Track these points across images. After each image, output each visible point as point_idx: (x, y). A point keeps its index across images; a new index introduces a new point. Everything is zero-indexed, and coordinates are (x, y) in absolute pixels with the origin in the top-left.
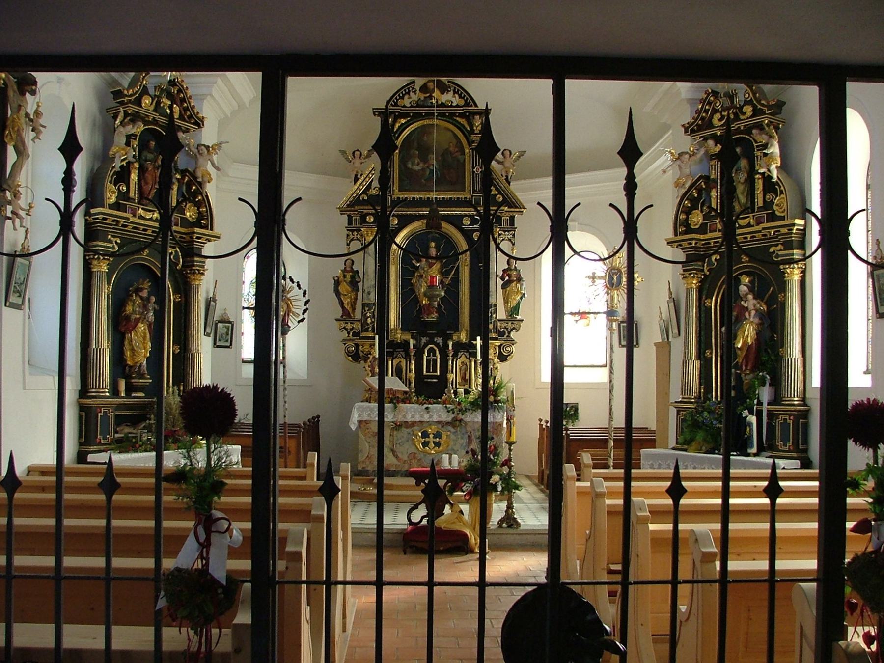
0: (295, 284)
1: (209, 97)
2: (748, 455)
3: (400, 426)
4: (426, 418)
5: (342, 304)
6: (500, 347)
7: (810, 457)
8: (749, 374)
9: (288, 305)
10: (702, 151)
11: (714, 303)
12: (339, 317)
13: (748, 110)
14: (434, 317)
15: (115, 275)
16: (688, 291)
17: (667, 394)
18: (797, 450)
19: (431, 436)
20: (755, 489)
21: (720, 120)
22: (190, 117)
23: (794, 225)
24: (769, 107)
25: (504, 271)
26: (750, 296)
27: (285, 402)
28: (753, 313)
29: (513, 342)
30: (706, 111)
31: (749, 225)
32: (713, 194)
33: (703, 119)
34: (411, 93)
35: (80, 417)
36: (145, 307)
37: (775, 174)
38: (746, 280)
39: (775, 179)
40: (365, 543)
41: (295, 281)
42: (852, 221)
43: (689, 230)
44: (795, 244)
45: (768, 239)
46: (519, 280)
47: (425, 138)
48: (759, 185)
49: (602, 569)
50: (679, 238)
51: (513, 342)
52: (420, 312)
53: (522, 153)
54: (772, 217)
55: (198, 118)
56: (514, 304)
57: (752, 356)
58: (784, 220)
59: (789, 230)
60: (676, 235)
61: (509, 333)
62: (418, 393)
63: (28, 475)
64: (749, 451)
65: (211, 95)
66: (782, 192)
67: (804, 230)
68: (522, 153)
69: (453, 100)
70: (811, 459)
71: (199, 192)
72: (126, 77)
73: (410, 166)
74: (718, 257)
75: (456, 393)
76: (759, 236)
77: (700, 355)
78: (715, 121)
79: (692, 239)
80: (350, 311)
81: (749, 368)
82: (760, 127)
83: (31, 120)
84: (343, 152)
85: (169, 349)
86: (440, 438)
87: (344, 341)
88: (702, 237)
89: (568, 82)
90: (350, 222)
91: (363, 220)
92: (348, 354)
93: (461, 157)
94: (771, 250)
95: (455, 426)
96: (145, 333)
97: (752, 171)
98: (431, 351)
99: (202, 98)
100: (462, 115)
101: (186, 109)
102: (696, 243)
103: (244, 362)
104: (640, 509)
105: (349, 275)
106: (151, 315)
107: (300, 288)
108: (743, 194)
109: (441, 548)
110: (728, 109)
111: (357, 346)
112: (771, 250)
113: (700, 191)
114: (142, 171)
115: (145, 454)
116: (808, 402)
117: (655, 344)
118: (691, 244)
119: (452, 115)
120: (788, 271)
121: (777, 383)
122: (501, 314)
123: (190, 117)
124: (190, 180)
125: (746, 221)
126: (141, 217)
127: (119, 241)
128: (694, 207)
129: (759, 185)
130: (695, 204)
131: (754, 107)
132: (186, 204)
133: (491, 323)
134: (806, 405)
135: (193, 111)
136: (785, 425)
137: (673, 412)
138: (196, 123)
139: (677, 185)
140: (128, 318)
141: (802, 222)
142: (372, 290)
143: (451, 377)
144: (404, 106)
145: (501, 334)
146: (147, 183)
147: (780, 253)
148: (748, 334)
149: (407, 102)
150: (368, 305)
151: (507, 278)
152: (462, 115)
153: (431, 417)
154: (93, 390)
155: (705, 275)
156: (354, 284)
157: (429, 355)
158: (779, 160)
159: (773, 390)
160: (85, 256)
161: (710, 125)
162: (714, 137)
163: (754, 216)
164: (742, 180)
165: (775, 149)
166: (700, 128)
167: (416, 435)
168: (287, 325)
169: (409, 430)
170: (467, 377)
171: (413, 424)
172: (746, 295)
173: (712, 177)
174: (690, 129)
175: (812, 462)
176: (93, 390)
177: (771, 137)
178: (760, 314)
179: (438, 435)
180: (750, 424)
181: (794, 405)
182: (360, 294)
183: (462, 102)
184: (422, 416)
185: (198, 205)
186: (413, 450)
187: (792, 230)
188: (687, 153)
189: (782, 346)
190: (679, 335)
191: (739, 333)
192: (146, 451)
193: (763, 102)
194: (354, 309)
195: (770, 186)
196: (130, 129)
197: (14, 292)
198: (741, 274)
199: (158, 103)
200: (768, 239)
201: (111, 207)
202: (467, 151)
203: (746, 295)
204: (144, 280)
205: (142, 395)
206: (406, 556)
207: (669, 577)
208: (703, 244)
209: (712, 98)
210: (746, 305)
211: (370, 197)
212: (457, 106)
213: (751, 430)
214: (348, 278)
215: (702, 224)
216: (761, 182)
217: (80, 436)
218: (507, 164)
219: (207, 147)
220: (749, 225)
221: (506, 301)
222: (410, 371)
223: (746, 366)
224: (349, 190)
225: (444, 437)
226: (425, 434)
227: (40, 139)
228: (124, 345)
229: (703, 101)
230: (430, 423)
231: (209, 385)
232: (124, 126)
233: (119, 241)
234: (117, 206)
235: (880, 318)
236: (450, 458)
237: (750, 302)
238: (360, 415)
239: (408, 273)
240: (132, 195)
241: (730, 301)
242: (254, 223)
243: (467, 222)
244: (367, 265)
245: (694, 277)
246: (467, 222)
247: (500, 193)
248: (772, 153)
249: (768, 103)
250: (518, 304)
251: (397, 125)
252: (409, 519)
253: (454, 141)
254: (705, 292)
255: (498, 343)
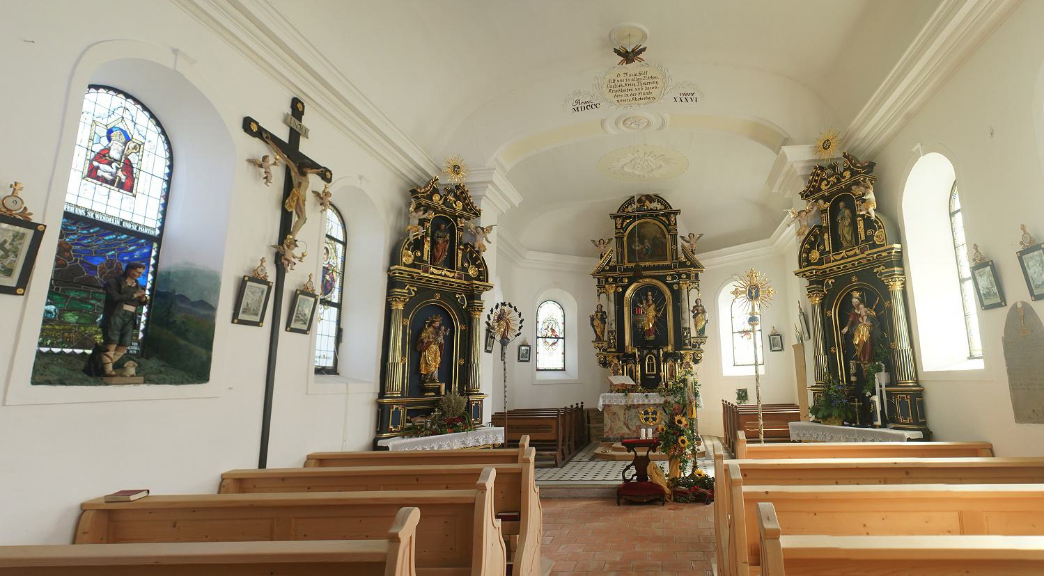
0: (518, 332)
1: (484, 197)
2: (875, 427)
3: (630, 407)
4: (646, 402)
5: (595, 332)
6: (693, 354)
7: (929, 428)
8: (867, 364)
9: (507, 323)
10: (815, 209)
11: (834, 313)
12: (594, 340)
13: (847, 174)
14: (652, 337)
15: (910, 107)
16: (813, 306)
17: (805, 380)
18: (916, 422)
19: (650, 413)
20: (896, 466)
21: (826, 185)
22: (471, 209)
23: (893, 248)
24: (863, 168)
25: (694, 307)
26: (862, 306)
27: (505, 397)
28: (865, 318)
29: (702, 351)
30: (816, 181)
31: (855, 255)
32: (826, 236)
33: (814, 187)
34: (633, 204)
35: (378, 412)
36: (437, 334)
37: (873, 214)
38: (856, 294)
39: (873, 218)
40: (593, 496)
41: (522, 317)
42: (338, 368)
43: (810, 264)
44: (894, 263)
45: (872, 263)
46: (704, 312)
47: (642, 231)
48: (861, 225)
49: (744, 563)
50: (803, 270)
51: (702, 351)
52: (644, 335)
53: (701, 235)
54: (874, 246)
55: (476, 210)
56: (701, 327)
57: (868, 350)
58: (616, 271)
59: (881, 255)
60: (801, 268)
61: (699, 345)
62: (642, 385)
63: (305, 466)
64: (875, 423)
65: (491, 182)
66: (880, 227)
67: (901, 252)
68: (701, 235)
69: (657, 206)
70: (931, 430)
71: (477, 258)
72: (183, 305)
73: (633, 247)
74: (834, 281)
75: (666, 385)
76: (864, 261)
77: (827, 351)
78: (823, 187)
79: (812, 270)
80: (601, 336)
81: (866, 359)
82: (857, 183)
83: (322, 198)
84: (593, 241)
85: (457, 361)
86: (656, 415)
87: (597, 355)
88: (820, 268)
89: (982, 360)
90: (599, 283)
91: (607, 280)
92: (600, 362)
93: (664, 240)
94: (875, 271)
95: (462, 419)
96: (656, 330)
97: (854, 216)
98: (650, 358)
99: (480, 198)
100: (663, 215)
101: (468, 204)
102: (816, 272)
103: (538, 370)
104: (768, 519)
105: (599, 314)
106: (441, 340)
107: (520, 317)
108: (848, 233)
109: (645, 501)
110: (833, 176)
111: (605, 357)
112: (875, 271)
113: (815, 237)
114: (434, 244)
115: (427, 438)
116: (921, 384)
117: (793, 346)
118: (812, 273)
119: (657, 215)
120: (891, 283)
121: (891, 369)
122: (694, 333)
123: (471, 209)
124: (471, 250)
125: (853, 252)
126: (433, 273)
127: (416, 289)
128: (812, 248)
129: (861, 225)
130: (813, 246)
131: (851, 170)
132: (108, 356)
133: (610, 332)
134: (920, 386)
135: (473, 206)
136: (903, 402)
137: (810, 394)
138: (475, 214)
139: (799, 234)
140: (422, 341)
141: (899, 246)
142: (613, 322)
143: (662, 374)
144: (629, 212)
145: (694, 346)
146: (438, 251)
147: (883, 271)
148: (862, 334)
149: (630, 209)
150: (611, 332)
151: (696, 312)
152: (663, 215)
153: (650, 401)
154: (389, 392)
155: (825, 294)
156: (603, 320)
157: (649, 361)
158: (875, 203)
159: (889, 376)
160: (387, 299)
161: (820, 189)
162: (823, 197)
163: (858, 248)
164: (847, 224)
165: (871, 196)
166: (812, 193)
167: (641, 414)
168: (507, 338)
169: (636, 410)
170: (674, 374)
171: (638, 406)
172: (858, 305)
173: (824, 225)
174: (805, 195)
175: (931, 432)
176: (389, 392)
177: (867, 188)
178: (870, 317)
179: (655, 413)
180: (874, 402)
181: (909, 386)
182: (606, 325)
183: (663, 207)
184: (644, 401)
185: (478, 266)
186: (638, 423)
187: (891, 253)
188: (803, 211)
189: (893, 340)
190: (810, 338)
191: (856, 334)
192: (426, 435)
193: (858, 165)
194: (603, 335)
195: (869, 223)
196: (420, 215)
197: (295, 320)
198: (853, 291)
199: (446, 199)
200: (872, 263)
201: (405, 265)
202: (667, 236)
203: (858, 305)
204: (437, 316)
205: (433, 394)
206: (618, 507)
207: (753, 363)
208: (821, 273)
209: (819, 172)
210: (859, 313)
211: (610, 267)
212: (660, 210)
213: (875, 407)
214: (599, 316)
215: (819, 259)
216: (862, 223)
217: (377, 427)
218: (692, 242)
219: (483, 229)
220: (855, 255)
221: (696, 326)
222: (638, 371)
223: (864, 358)
224: (597, 263)
225: (658, 414)
226: (646, 413)
227: (1023, 228)
228: (420, 360)
229: (813, 174)
230: (649, 405)
231: (811, 147)
232: (416, 212)
233: (416, 289)
234: (413, 265)
235: (986, 309)
236: (646, 431)
237: (862, 310)
238: (603, 401)
239: (634, 311)
240: (425, 258)
241: (846, 308)
242: (322, 181)
243: (669, 279)
244: (610, 309)
245: (816, 296)
246: (669, 279)
247: (689, 260)
248: (869, 199)
249: (862, 165)
250: (704, 327)
251: (625, 223)
252: (624, 477)
253: (660, 231)
254: (826, 306)
255: (692, 352)
